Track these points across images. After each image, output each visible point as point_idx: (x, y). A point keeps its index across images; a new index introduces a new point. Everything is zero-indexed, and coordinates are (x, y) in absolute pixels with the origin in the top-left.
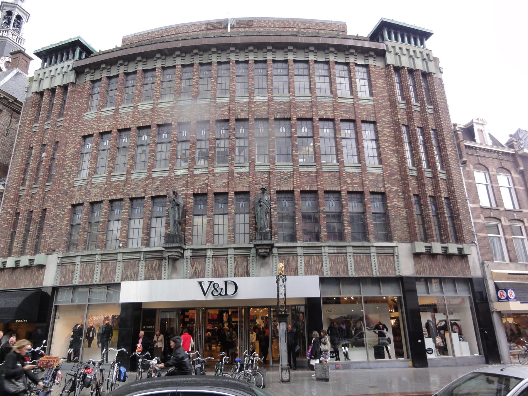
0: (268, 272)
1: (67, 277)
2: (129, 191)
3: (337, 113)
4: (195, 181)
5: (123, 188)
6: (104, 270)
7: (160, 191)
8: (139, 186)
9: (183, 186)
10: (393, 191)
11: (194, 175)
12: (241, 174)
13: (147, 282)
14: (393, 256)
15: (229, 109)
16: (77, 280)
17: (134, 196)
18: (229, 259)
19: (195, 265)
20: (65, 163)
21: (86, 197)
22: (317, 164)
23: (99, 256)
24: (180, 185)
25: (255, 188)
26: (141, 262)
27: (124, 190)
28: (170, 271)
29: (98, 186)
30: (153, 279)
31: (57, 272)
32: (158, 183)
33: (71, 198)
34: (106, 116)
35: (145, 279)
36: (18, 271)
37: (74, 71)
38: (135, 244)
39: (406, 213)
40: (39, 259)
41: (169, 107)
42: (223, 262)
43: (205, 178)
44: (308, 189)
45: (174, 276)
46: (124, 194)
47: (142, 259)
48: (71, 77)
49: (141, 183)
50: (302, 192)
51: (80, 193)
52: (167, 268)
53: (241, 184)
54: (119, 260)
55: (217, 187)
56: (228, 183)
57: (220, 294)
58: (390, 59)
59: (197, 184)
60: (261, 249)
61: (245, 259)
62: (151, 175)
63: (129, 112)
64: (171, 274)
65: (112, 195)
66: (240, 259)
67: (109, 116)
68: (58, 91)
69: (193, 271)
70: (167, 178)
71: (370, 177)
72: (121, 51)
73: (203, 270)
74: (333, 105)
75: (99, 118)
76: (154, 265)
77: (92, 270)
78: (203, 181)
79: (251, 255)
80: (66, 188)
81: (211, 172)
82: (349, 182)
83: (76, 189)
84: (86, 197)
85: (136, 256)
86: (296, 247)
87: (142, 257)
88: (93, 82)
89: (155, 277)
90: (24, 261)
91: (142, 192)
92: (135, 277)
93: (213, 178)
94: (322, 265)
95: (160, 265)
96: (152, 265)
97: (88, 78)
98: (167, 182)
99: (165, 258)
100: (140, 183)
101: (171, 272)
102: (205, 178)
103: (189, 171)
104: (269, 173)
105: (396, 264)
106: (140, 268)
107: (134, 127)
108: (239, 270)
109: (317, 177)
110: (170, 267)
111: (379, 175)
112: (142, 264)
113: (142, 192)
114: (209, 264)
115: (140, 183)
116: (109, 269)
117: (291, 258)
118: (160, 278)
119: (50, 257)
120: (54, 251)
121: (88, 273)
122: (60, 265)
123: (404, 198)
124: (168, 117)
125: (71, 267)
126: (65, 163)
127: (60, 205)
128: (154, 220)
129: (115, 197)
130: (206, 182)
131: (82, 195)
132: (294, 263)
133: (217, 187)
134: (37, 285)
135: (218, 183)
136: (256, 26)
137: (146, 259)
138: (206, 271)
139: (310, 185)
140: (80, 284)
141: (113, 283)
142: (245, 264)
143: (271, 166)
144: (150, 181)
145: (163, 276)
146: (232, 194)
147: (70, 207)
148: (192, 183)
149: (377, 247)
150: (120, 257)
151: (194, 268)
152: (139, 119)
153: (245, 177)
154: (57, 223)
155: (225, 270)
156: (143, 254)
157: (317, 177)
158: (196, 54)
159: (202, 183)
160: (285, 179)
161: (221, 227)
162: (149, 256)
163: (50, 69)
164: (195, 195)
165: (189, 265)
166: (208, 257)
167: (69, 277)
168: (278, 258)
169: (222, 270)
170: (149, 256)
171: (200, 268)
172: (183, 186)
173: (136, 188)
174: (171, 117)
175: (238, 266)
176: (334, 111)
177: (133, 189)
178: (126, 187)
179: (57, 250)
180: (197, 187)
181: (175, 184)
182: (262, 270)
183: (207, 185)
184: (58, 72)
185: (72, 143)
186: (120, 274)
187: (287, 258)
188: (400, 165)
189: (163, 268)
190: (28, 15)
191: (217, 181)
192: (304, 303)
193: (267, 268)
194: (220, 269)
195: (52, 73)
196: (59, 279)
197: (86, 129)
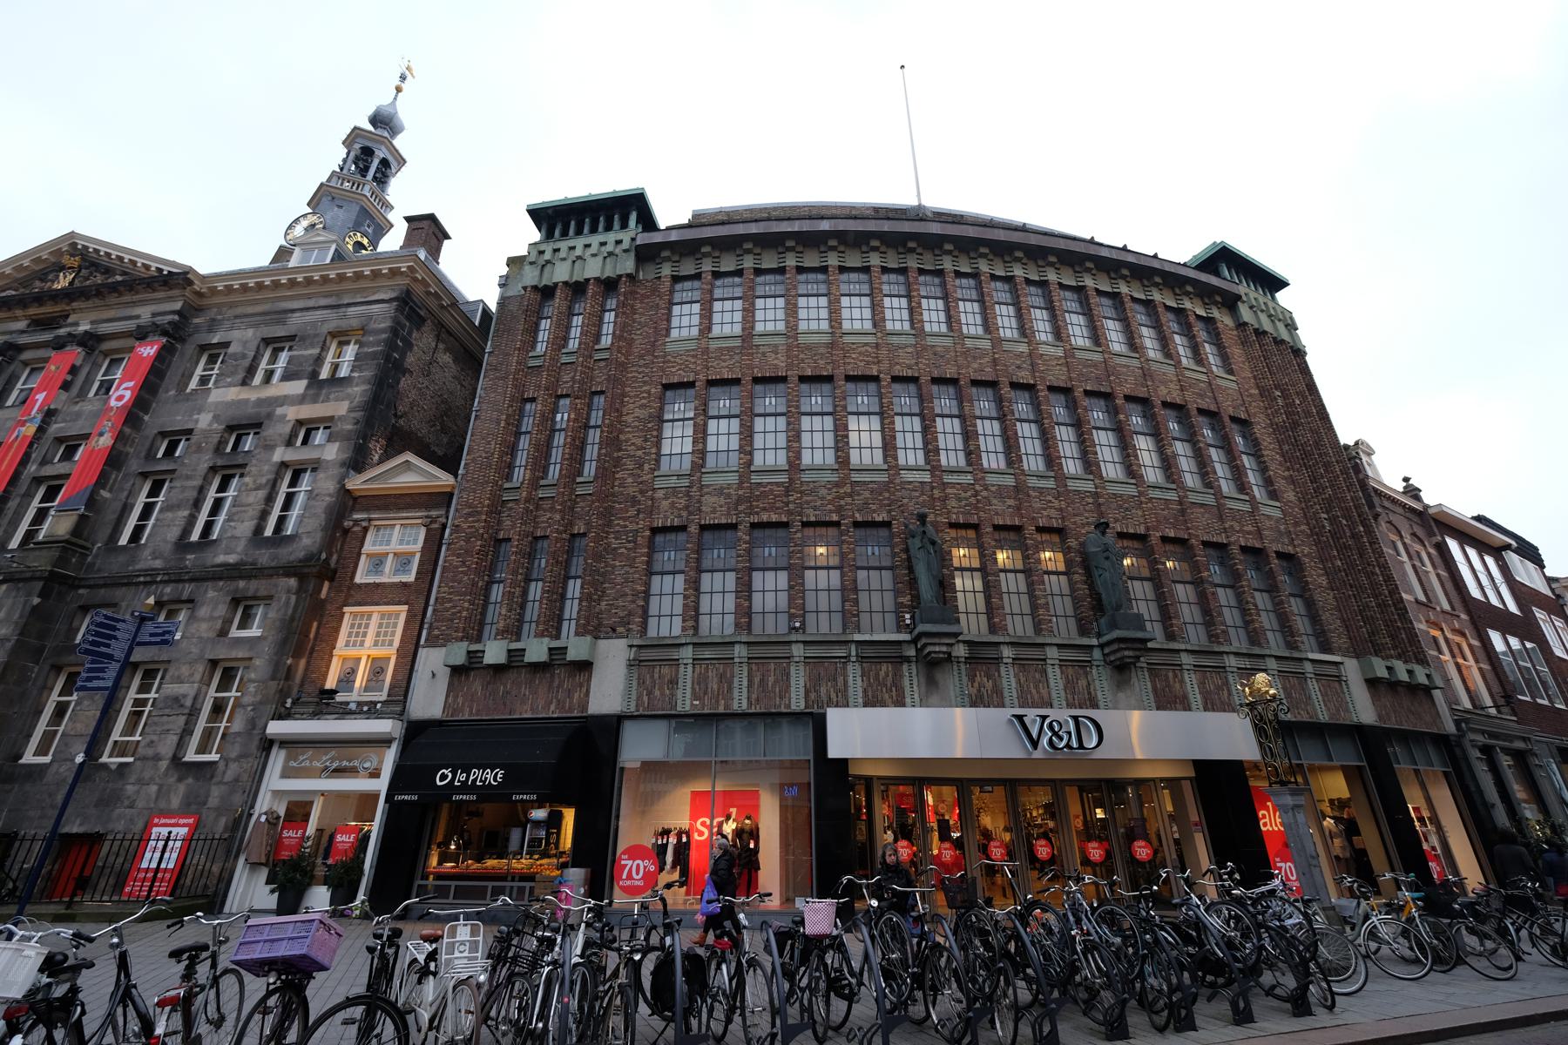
1: (657, 693)
3: (1189, 396)
6: (757, 680)
8: (823, 498)
10: (1304, 550)
12: (1041, 490)
15: (995, 362)
16: (688, 702)
17: (813, 519)
19: (978, 679)
20: (622, 437)
21: (690, 513)
26: (850, 667)
27: (787, 504)
29: (720, 491)
31: (629, 679)
33: (650, 512)
35: (866, 705)
36: (512, 675)
37: (633, 254)
40: (577, 648)
44: (1172, 534)
45: (934, 699)
46: (790, 513)
48: (628, 265)
56: (1019, 508)
62: (848, 476)
66: (1070, 671)
67: (729, 349)
68: (591, 289)
70: (886, 486)
71: (1268, 523)
72: (720, 228)
73: (997, 691)
76: (882, 673)
77: (726, 681)
80: (631, 491)
83: (660, 494)
84: (690, 513)
85: (840, 652)
88: (676, 279)
90: (537, 650)
91: (831, 511)
93: (985, 493)
95: (898, 676)
96: (877, 675)
97: (666, 270)
99: (907, 660)
100: (823, 492)
106: (850, 679)
107: (793, 374)
108: (1074, 693)
109: (1183, 512)
111: (1278, 520)
112: (854, 674)
113: (831, 511)
114: (1009, 679)
115: (823, 492)
116: (771, 679)
117: (1171, 674)
118: (901, 703)
119: (602, 644)
120: (614, 630)
122: (633, 664)
124: (868, 363)
125: (666, 670)
126: (622, 437)
128: (656, 580)
130: (973, 500)
135: (997, 505)
137: (861, 659)
138: (1006, 694)
141: (784, 710)
142: (1082, 683)
145: (908, 700)
147: (648, 533)
149: (1312, 661)
150: (798, 651)
154: (614, 567)
155: (1044, 692)
156: (853, 647)
157: (1183, 512)
158: (912, 250)
162: (869, 652)
163: (571, 243)
165: (965, 679)
167: (662, 694)
170: (869, 652)
171: (989, 685)
175: (1070, 685)
177: (808, 503)
179: (620, 629)
182: (1121, 695)
183: (977, 508)
184: (594, 249)
189: (906, 682)
190: (402, 162)
191: (995, 501)
195: (578, 252)
196: (634, 697)
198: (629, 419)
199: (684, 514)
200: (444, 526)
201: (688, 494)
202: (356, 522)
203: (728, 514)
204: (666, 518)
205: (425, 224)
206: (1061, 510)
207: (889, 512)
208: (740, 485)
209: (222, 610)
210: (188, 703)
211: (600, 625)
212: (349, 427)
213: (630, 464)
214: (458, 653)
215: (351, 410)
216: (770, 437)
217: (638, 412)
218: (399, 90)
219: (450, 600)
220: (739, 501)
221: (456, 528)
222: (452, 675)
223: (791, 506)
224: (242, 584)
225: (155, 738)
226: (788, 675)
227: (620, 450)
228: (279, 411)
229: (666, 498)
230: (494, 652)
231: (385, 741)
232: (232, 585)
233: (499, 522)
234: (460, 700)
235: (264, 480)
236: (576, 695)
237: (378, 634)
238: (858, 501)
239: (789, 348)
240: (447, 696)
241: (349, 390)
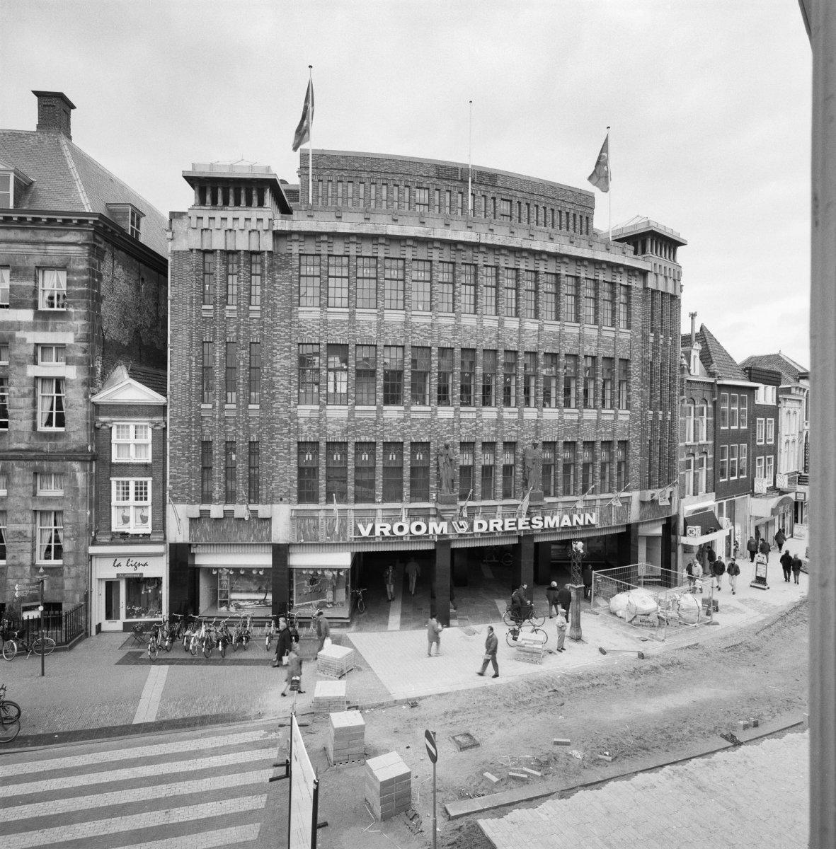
2: (382, 433)
4: (461, 427)
5: (374, 429)
8: (395, 428)
9: (448, 432)
11: (460, 420)
17: (389, 441)
27: (376, 431)
34: (334, 320)
41: (425, 324)
48: (267, 243)
50: (565, 443)
51: (310, 427)
55: (485, 436)
58: (651, 283)
59: (463, 430)
63: (370, 322)
67: (341, 322)
70: (429, 421)
74: (598, 340)
75: (325, 322)
80: (283, 416)
93: (481, 425)
100: (395, 424)
103: (455, 415)
109: (578, 426)
120: (281, 500)
125: (311, 521)
127: (277, 440)
129: (363, 439)
130: (474, 429)
131: (314, 432)
133: (485, 436)
134: (262, 540)
136: (500, 185)
144: (409, 423)
146: (500, 446)
148: (458, 429)
152: (387, 333)
154: (277, 463)
157: (578, 426)
164: (462, 444)
172: (448, 432)
174: (429, 338)
176: (598, 346)
177: (386, 431)
178: (378, 429)
179: (284, 499)
185: (281, 350)
196: (296, 534)
197: (305, 333)
198: (278, 366)
199: (317, 434)
200: (165, 429)
201: (318, 422)
202: (104, 424)
204: (306, 436)
205: (55, 101)
206: (517, 431)
207: (430, 436)
208: (349, 420)
209: (29, 480)
210: (29, 535)
211: (273, 496)
212: (80, 355)
213: (281, 398)
214: (195, 510)
215: (77, 340)
216: (338, 295)
217: (284, 362)
218: (434, 759)
219: (180, 478)
220: (347, 430)
221: (174, 432)
222: (191, 525)
223: (378, 433)
224: (37, 463)
225: (16, 554)
227: (274, 388)
228: (18, 335)
229: (306, 424)
230: (216, 511)
231: (161, 555)
232: (31, 464)
233: (202, 430)
234: (198, 533)
235: (26, 390)
236: (264, 532)
237: (136, 494)
238: (415, 429)
239: (379, 324)
240: (190, 531)
241: (70, 323)
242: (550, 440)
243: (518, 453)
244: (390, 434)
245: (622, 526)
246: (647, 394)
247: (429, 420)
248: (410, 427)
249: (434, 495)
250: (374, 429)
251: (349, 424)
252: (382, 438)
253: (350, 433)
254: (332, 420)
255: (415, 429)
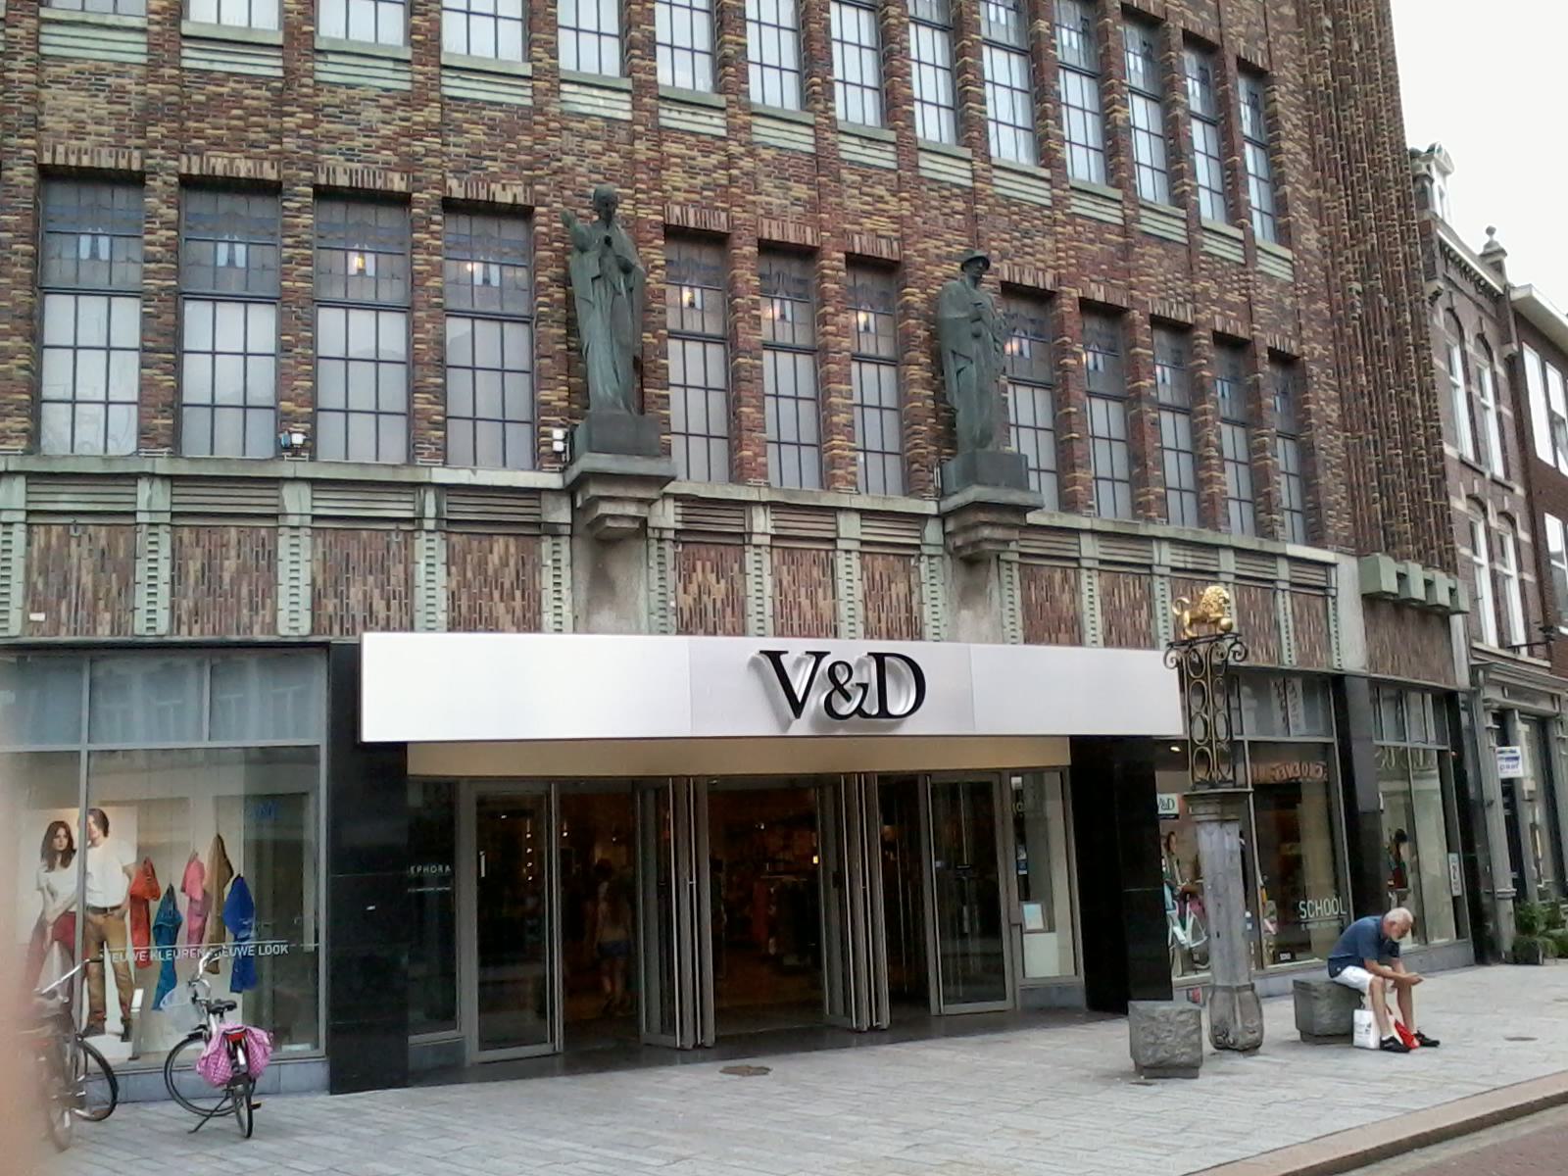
0: (985, 626)
5: (273, 123)
6: (194, 567)
7: (494, 178)
8: (369, 131)
11: (661, 134)
13: (681, 647)
14: (1325, 597)
17: (342, 181)
18: (841, 561)
19: (698, 576)
22: (1125, 196)
23: (305, 490)
24: (595, 170)
25: (923, 253)
26: (421, 542)
27: (278, 136)
28: (582, 596)
29: (94, 79)
30: (492, 626)
32: (478, 133)
38: (363, 440)
39: (1346, 445)
42: (816, 573)
43: (714, 159)
45: (605, 617)
46: (283, 159)
47: (430, 525)
49: (378, 114)
52: (566, 573)
53: (868, 224)
54: (294, 521)
55: (769, 214)
57: (859, 710)
60: (992, 524)
61: (899, 566)
64: (589, 613)
65: (199, 152)
69: (688, 601)
70: (527, 118)
76: (494, 559)
78: (707, 171)
79: (926, 550)
81: (742, 136)
82: (1214, 295)
86: (1076, 532)
87: (430, 511)
89: (508, 624)
91: (388, 167)
92: (394, 612)
93: (747, 163)
94: (1151, 615)
95: (528, 566)
98: (526, 140)
100: (371, 114)
101: (589, 602)
102: (714, 159)
103: (636, 107)
104: (972, 195)
105: (1333, 630)
106: (421, 568)
108: (879, 610)
109: (1126, 250)
110: (583, 577)
112: (429, 555)
113: (388, 167)
114: (760, 577)
116: (231, 565)
117: (1058, 576)
118: (530, 623)
121: (87, 580)
123: (1340, 389)
130: (721, 176)
132: (1066, 597)
133: (769, 214)
137: (448, 525)
139: (1107, 280)
140: (37, 639)
143: (978, 164)
144: (432, 114)
145: (548, 618)
151: (693, 588)
153: (880, 190)
155: (825, 605)
156: (430, 499)
157: (1126, 250)
159: (700, 180)
160: (1026, 234)
161: (362, 425)
162: (468, 510)
165: (671, 576)
166: (756, 540)
168: (1016, 574)
169: (814, 605)
171: (719, 589)
173: (350, 136)
175: (875, 592)
177: (331, 138)
178: (289, 123)
180: (680, 196)
181: (569, 160)
186: (305, 594)
187: (1046, 572)
188: (1328, 262)
189: (547, 580)
192: (1065, 759)
193: (980, 608)
194: (805, 603)
203: (119, 145)
206: (898, 219)
207: (530, 183)
220: (149, 113)
223: (290, 143)
226: (272, 556)
238: (457, 147)
242: (1028, 281)
243: (907, 306)
244: (350, 155)
245: (279, 1131)
246: (1338, 206)
247: (526, 113)
248: (438, 130)
249: (558, 434)
250: (273, 123)
251: (153, 89)
252: (311, 165)
253: (155, 132)
254: (68, 69)
255: (457, 147)
